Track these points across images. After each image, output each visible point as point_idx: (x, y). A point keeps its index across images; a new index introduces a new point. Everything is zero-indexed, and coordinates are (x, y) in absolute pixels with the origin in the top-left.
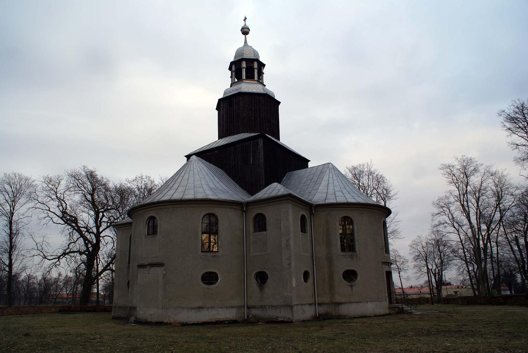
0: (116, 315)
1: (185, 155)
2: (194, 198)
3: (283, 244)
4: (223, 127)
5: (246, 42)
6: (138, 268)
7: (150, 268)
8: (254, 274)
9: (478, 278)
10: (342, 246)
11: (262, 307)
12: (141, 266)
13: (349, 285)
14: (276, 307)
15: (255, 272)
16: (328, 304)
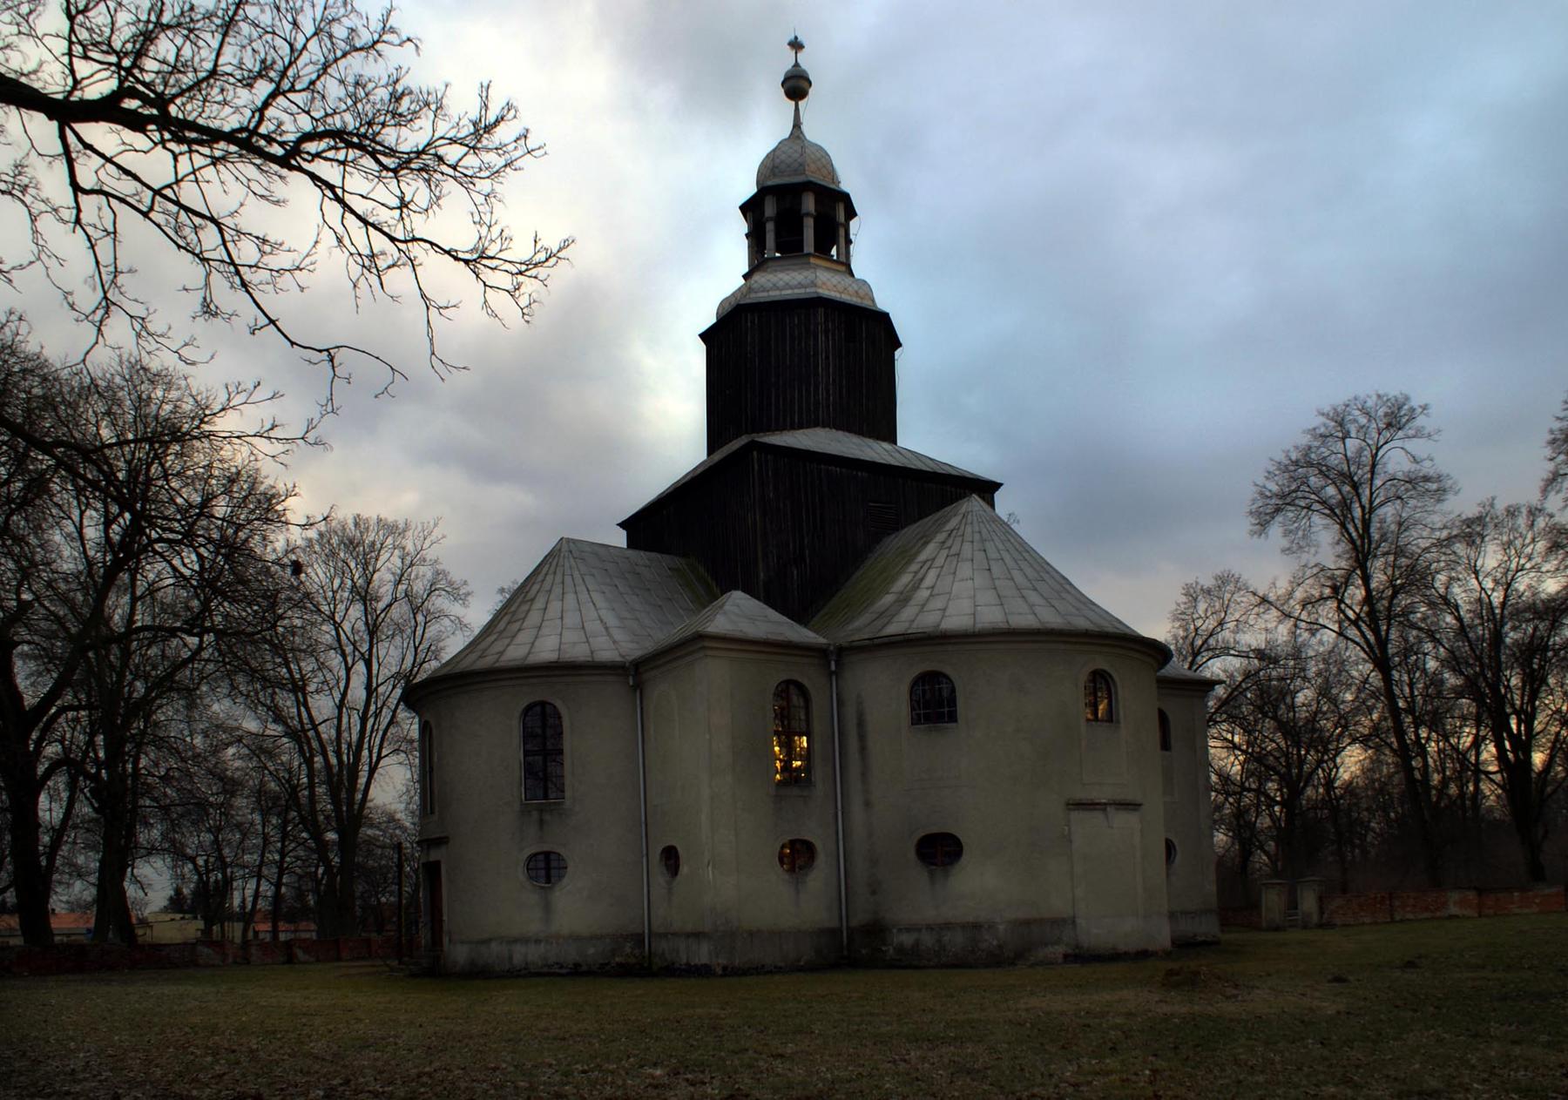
0: (737, 961)
1: (620, 521)
2: (971, 622)
5: (797, 125)
9: (1550, 795)
12: (1131, 806)
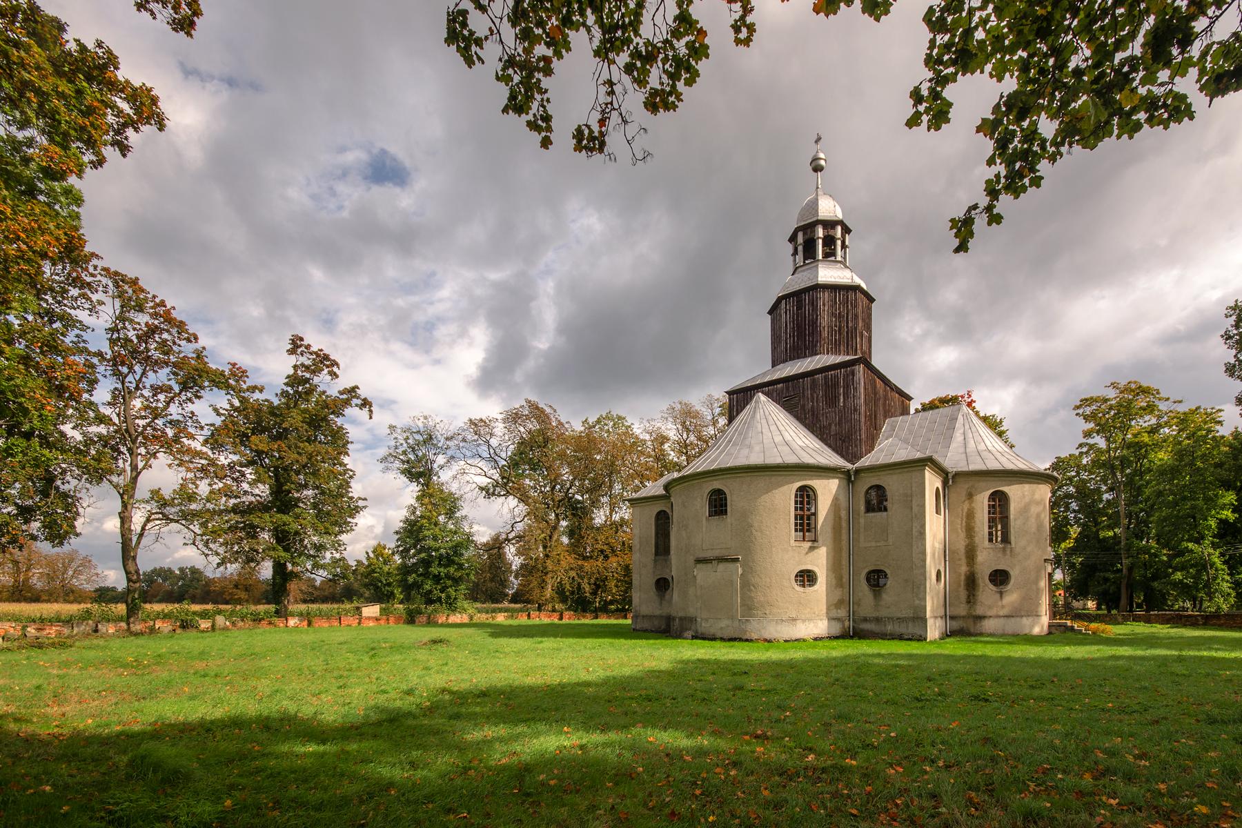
3: (914, 530)
4: (786, 344)
11: (878, 620)
14: (901, 620)
15: (866, 571)
16: (963, 617)
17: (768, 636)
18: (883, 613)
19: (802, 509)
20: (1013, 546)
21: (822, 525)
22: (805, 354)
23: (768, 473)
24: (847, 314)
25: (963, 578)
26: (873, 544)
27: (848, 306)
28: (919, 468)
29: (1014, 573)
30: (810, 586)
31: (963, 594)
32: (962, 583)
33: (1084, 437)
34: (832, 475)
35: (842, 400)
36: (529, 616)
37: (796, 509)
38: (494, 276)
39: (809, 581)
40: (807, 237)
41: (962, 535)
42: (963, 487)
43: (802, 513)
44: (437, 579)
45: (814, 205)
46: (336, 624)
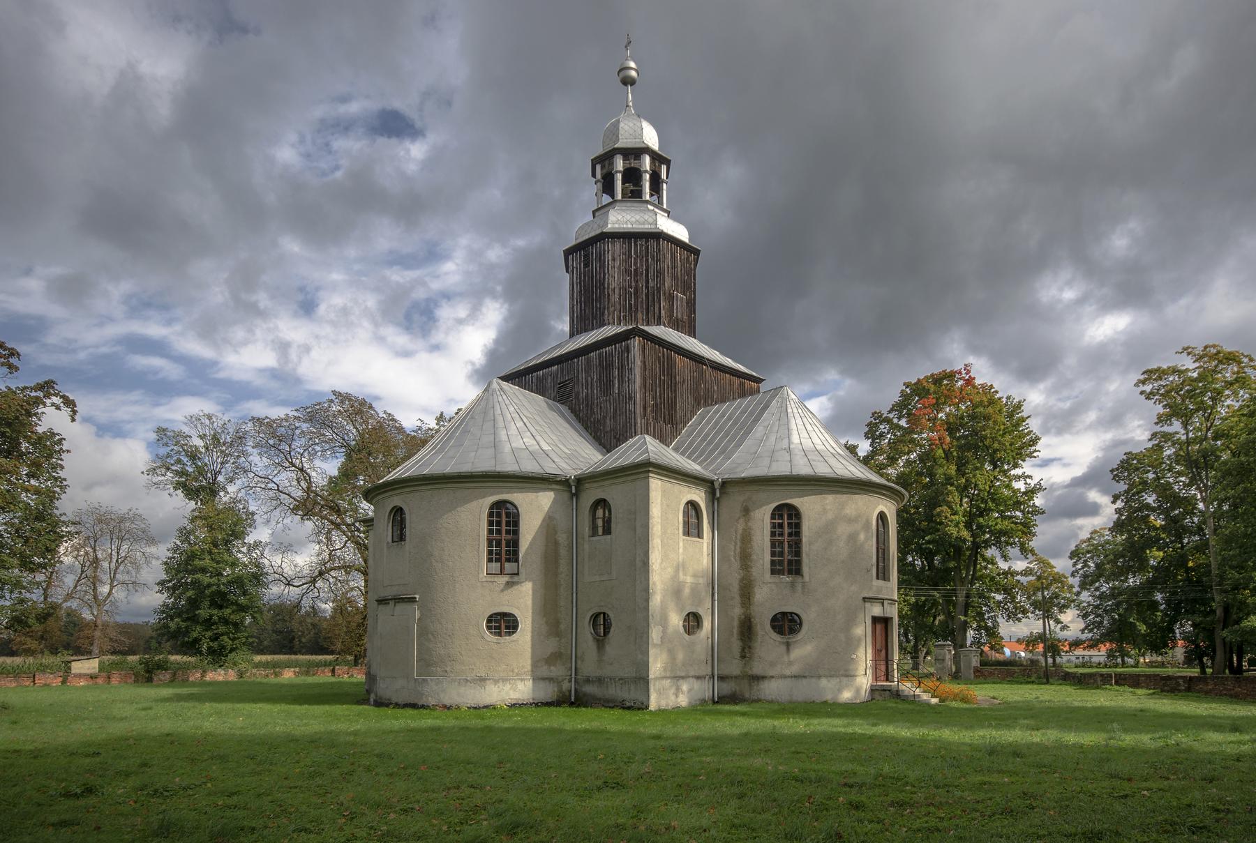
3: (638, 559)
6: (379, 604)
7: (395, 605)
8: (589, 618)
10: (490, 552)
11: (600, 681)
13: (783, 643)
17: (447, 702)
18: (607, 671)
19: (499, 532)
20: (807, 578)
21: (526, 553)
22: (593, 325)
23: (449, 485)
24: (647, 271)
25: (736, 623)
26: (597, 578)
27: (647, 260)
28: (642, 476)
29: (809, 616)
30: (510, 634)
31: (736, 645)
32: (735, 631)
33: (1157, 424)
34: (543, 486)
35: (617, 386)
36: (333, 671)
37: (490, 532)
38: (521, 243)
39: (507, 628)
40: (605, 171)
41: (736, 564)
42: (735, 500)
43: (498, 537)
44: (208, 623)
45: (614, 131)
46: (28, 682)
